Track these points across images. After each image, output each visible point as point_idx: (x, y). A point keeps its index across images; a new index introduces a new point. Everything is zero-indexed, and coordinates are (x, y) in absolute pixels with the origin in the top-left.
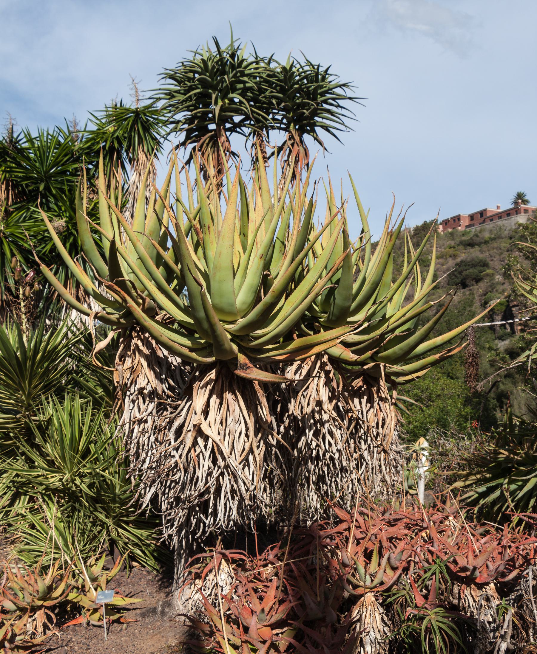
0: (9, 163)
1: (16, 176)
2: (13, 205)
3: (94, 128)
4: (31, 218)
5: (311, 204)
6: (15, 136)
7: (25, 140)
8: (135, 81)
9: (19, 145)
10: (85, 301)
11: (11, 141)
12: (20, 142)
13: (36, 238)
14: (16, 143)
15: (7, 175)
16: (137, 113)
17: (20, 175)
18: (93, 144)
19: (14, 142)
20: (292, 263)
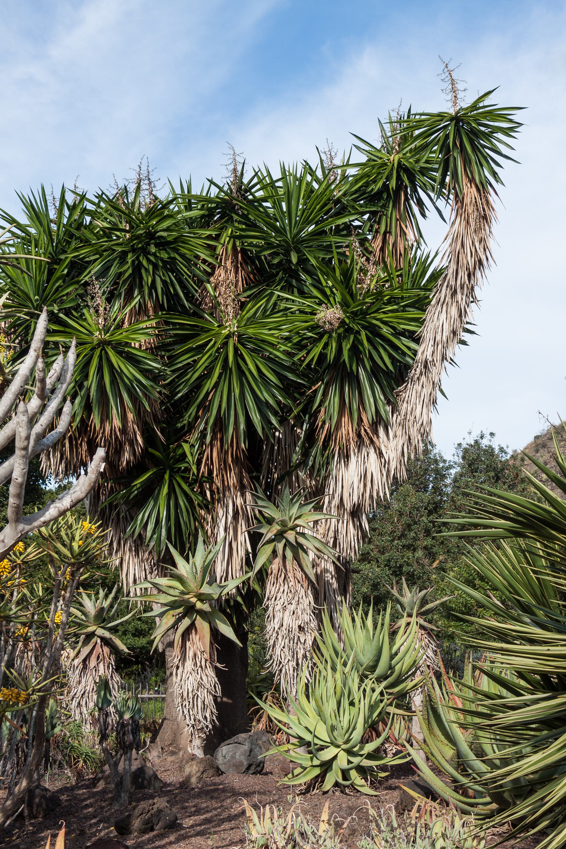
0: (236, 224)
1: (250, 244)
2: (244, 291)
3: (363, 159)
4: (274, 310)
5: (308, 540)
6: (245, 180)
7: (258, 187)
8: (451, 67)
9: (252, 194)
10: (372, 442)
11: (239, 189)
12: (253, 190)
13: (290, 342)
14: (246, 191)
15: (238, 244)
16: (457, 119)
17: (255, 241)
18: (367, 185)
19: (242, 190)
20: (376, 628)
